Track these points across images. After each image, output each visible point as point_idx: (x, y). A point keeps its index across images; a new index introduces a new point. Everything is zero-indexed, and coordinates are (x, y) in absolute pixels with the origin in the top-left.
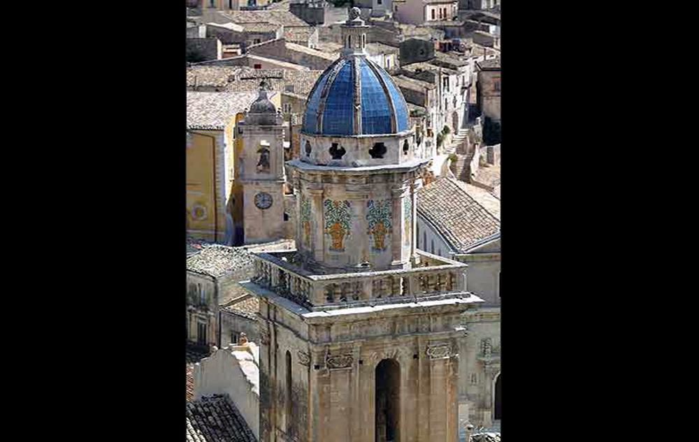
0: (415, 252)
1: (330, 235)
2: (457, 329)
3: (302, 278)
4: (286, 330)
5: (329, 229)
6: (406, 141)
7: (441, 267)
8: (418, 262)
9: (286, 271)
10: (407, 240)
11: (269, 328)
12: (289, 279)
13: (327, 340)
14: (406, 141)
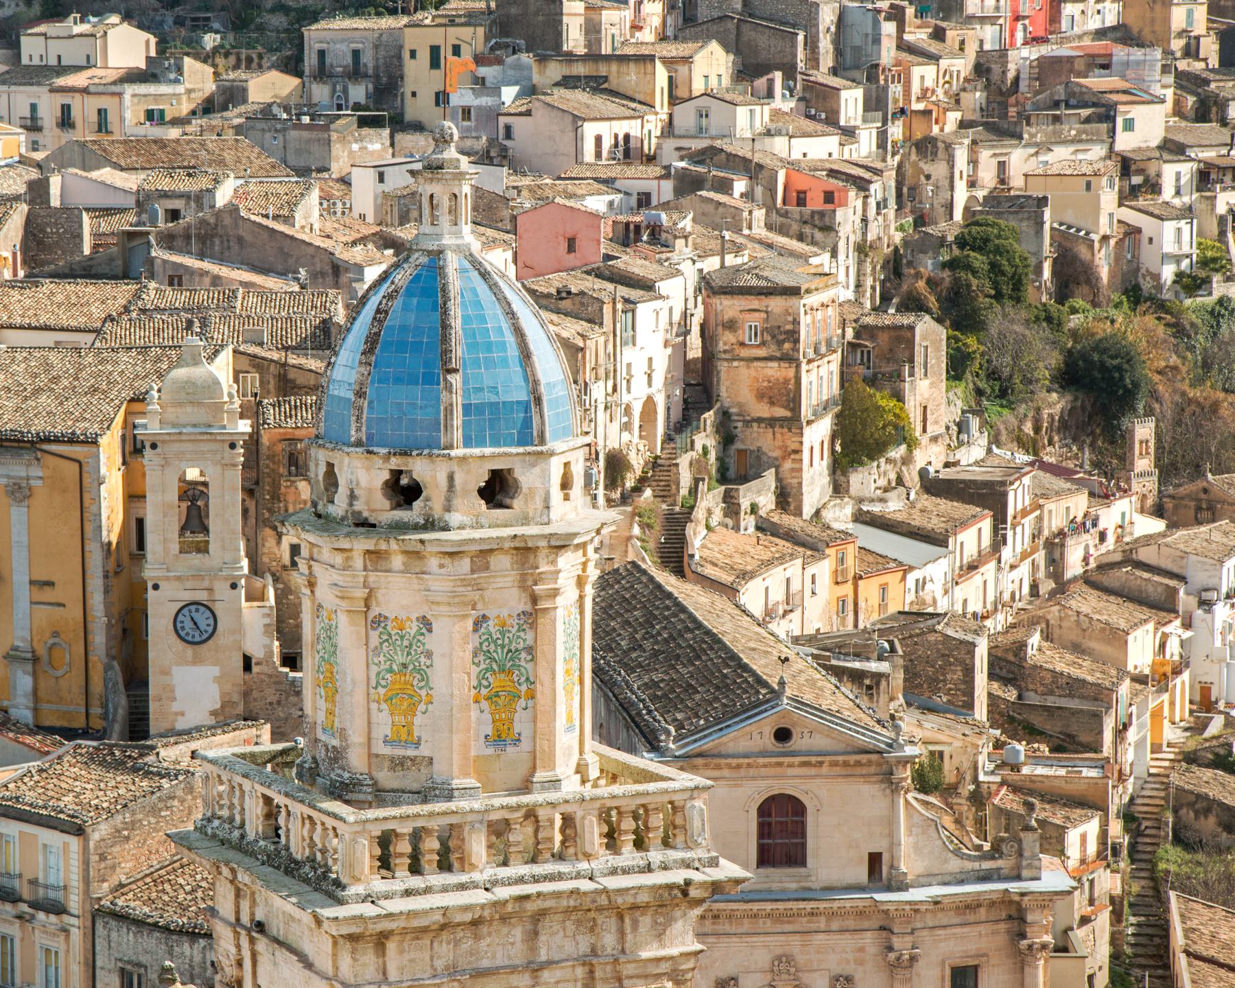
0: (587, 748)
1: (384, 706)
2: (645, 954)
3: (315, 814)
4: (282, 954)
5: (382, 691)
6: (567, 465)
7: (652, 787)
8: (594, 773)
9: (279, 799)
10: (570, 718)
11: (238, 947)
12: (287, 820)
13: (862, 875)
14: (567, 465)
